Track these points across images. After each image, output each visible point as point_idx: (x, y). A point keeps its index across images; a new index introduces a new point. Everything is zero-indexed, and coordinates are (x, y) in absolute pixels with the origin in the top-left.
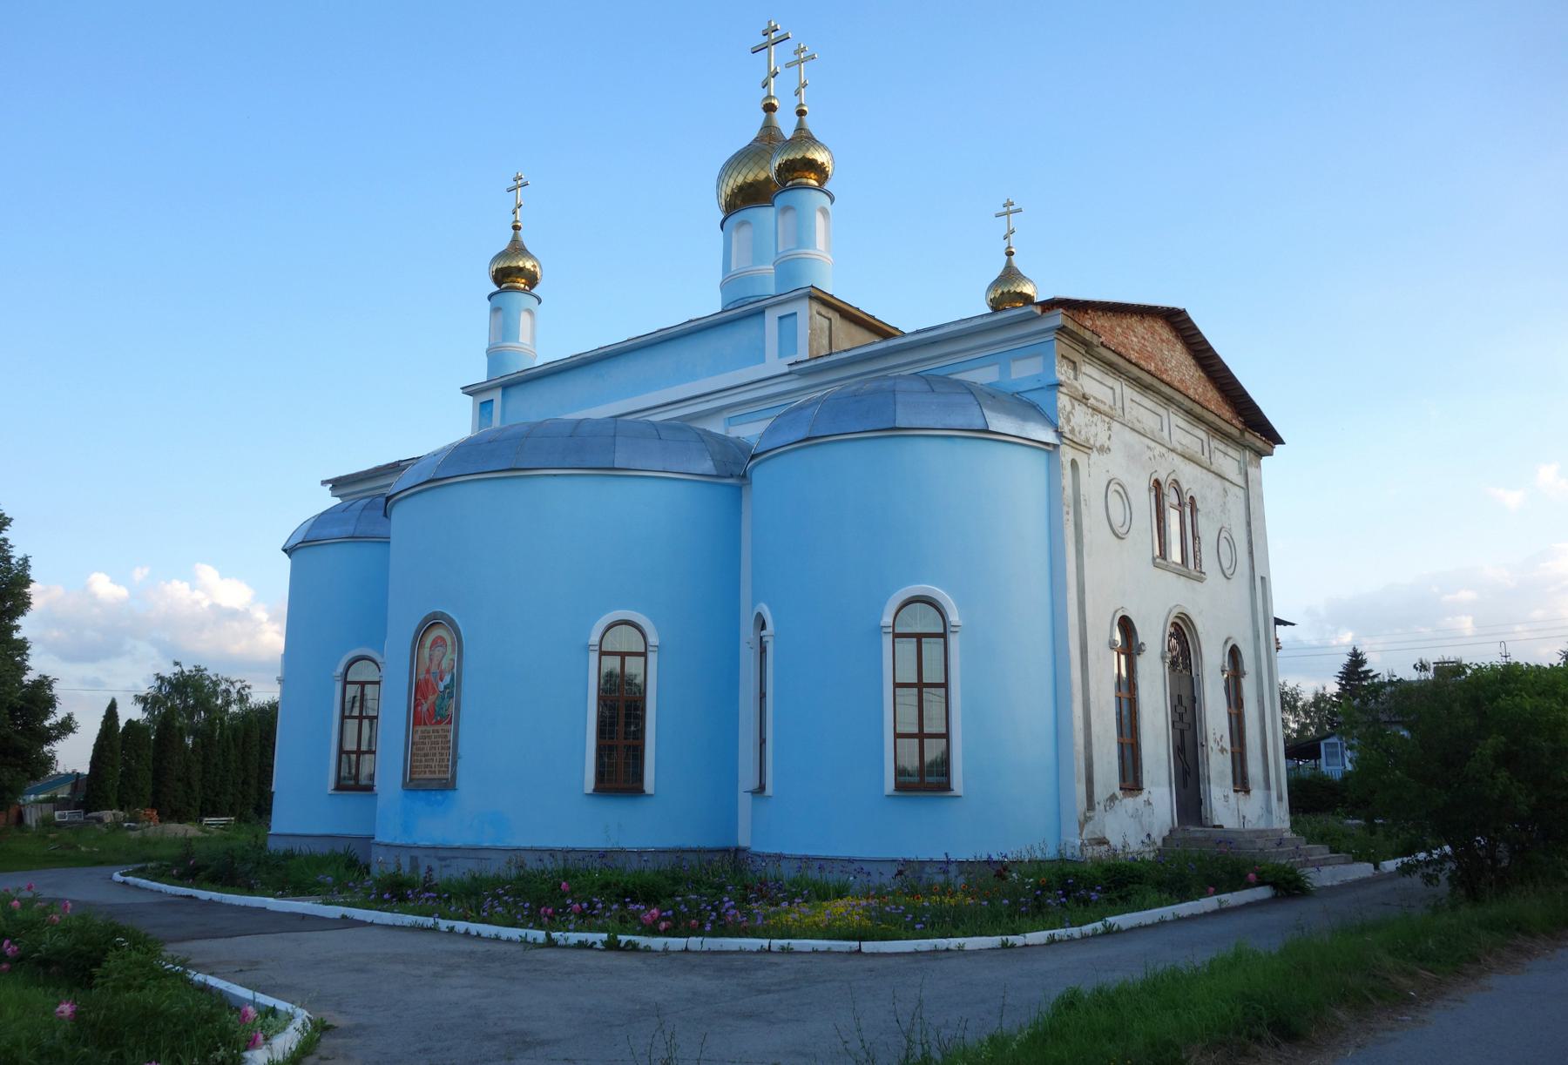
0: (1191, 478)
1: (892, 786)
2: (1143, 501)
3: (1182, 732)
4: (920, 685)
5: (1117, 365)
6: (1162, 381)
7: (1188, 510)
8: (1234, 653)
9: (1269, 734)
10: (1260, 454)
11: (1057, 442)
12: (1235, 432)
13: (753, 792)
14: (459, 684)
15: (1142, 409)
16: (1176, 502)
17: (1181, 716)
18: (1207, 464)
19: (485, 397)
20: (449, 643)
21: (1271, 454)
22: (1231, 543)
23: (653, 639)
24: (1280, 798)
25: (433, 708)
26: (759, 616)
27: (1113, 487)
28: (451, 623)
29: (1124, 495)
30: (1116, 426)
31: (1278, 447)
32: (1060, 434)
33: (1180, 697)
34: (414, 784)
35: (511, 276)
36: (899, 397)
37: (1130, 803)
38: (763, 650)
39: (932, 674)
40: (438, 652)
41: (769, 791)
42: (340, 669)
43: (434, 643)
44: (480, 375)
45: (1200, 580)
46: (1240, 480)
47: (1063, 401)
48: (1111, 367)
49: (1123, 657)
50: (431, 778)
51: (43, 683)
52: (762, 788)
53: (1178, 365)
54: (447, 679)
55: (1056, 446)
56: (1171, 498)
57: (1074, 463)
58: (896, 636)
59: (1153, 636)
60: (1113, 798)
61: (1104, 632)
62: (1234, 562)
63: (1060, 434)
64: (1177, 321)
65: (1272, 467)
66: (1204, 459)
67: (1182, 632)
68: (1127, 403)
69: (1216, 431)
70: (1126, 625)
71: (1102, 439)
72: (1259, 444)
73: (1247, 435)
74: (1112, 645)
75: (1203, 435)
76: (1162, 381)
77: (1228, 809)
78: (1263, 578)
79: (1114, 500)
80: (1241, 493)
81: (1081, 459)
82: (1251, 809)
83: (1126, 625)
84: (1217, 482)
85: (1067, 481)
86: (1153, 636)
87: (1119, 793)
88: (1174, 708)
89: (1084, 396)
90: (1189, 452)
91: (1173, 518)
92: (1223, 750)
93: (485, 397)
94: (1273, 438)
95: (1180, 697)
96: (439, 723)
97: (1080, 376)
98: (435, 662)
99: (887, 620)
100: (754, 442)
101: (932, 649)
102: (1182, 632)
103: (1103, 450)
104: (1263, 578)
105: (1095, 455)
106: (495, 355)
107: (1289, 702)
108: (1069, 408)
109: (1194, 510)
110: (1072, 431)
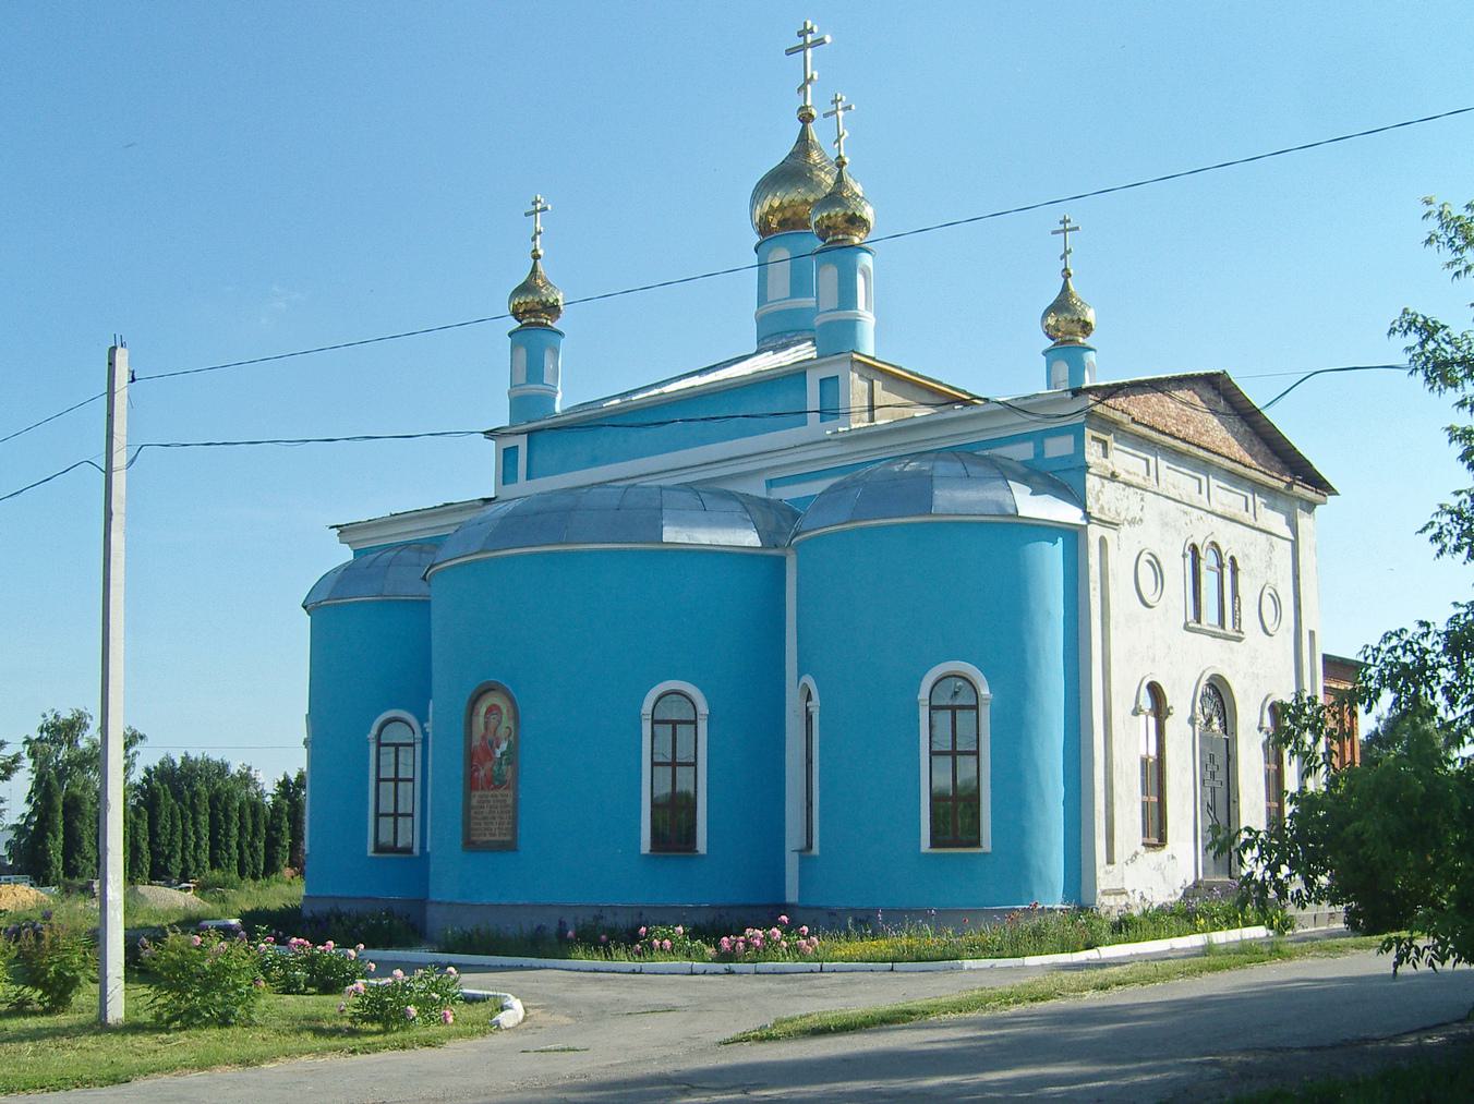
0: (1233, 540)
1: (649, 848)
2: (1177, 571)
3: (1213, 790)
4: (954, 753)
5: (1143, 441)
7: (1227, 572)
10: (1310, 506)
11: (1084, 523)
12: (1282, 485)
13: (800, 851)
16: (1214, 564)
18: (1251, 521)
19: (509, 442)
20: (505, 711)
23: (703, 708)
27: (1145, 557)
28: (506, 693)
29: (1156, 564)
32: (1087, 516)
33: (1212, 758)
35: (534, 314)
36: (935, 482)
37: (1154, 857)
40: (493, 720)
42: (374, 732)
43: (489, 711)
44: (502, 419)
45: (1239, 640)
46: (1287, 532)
47: (1092, 482)
51: (186, 759)
53: (1217, 433)
54: (504, 746)
56: (1208, 559)
59: (1181, 701)
63: (1087, 516)
64: (1218, 389)
66: (1248, 518)
69: (1257, 487)
70: (1155, 690)
71: (1135, 512)
72: (1310, 495)
76: (1199, 446)
81: (1109, 534)
84: (1264, 535)
86: (1181, 701)
88: (1204, 765)
90: (1229, 512)
91: (1209, 581)
93: (509, 442)
96: (496, 788)
98: (491, 729)
102: (1218, 694)
104: (1312, 634)
105: (1125, 529)
106: (519, 404)
108: (1098, 487)
109: (1235, 571)
110: (1102, 509)
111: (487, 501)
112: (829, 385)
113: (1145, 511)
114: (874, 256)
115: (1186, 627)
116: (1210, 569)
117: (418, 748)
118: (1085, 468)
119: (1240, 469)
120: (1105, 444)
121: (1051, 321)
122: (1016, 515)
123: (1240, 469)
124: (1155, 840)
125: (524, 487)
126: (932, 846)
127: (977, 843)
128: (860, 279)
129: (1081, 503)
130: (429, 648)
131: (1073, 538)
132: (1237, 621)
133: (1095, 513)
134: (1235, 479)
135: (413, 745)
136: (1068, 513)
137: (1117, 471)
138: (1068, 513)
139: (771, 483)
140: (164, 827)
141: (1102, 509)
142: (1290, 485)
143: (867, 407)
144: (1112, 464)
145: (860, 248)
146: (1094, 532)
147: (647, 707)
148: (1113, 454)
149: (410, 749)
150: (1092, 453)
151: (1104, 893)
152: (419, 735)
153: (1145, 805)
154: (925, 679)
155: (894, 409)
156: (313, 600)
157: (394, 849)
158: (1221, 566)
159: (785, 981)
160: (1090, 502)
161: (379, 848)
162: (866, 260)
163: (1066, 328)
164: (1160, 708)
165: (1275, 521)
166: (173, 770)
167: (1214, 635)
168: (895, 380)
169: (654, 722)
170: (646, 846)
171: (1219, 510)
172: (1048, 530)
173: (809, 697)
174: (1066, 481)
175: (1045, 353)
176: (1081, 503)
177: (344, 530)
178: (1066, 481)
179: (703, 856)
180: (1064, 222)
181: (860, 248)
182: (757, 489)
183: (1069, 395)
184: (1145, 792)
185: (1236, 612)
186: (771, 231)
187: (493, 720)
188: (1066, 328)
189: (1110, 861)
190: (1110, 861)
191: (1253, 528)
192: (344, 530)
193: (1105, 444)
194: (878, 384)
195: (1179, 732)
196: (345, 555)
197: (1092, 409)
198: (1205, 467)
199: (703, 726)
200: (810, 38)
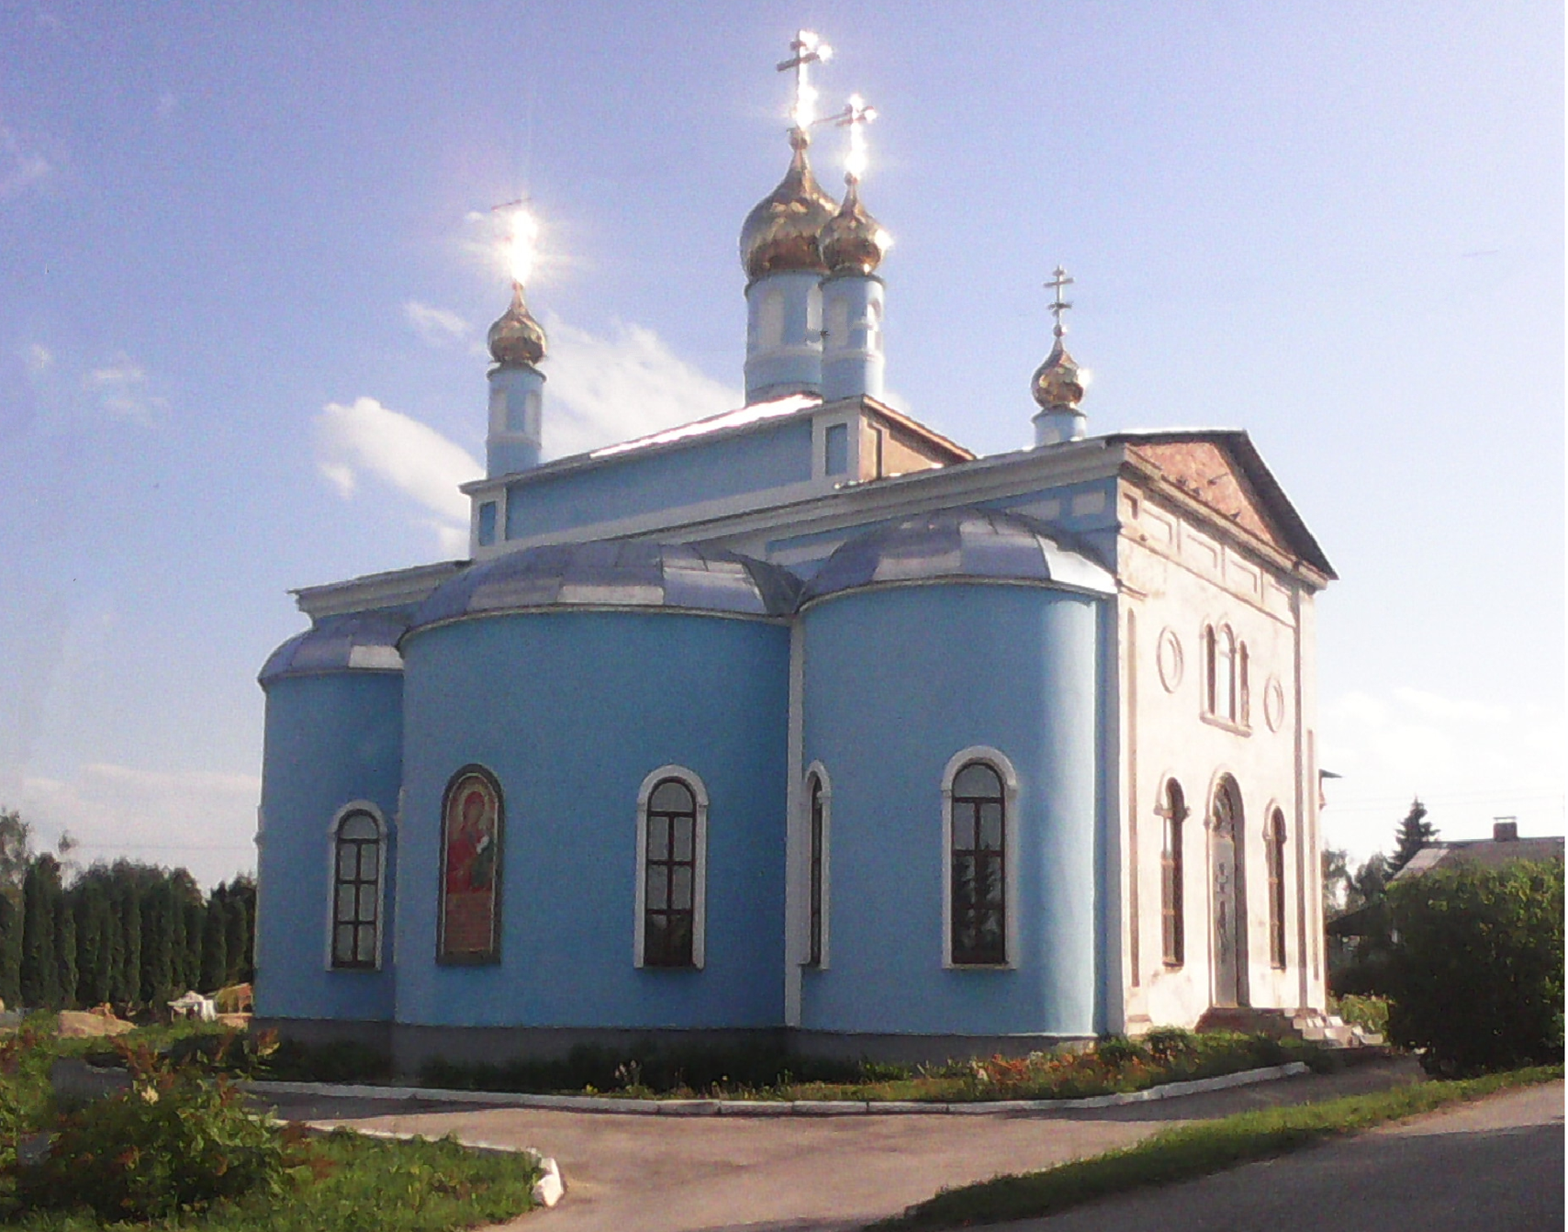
3: (1222, 904)
6: (1218, 512)
8: (1278, 818)
9: (1314, 902)
10: (1312, 589)
11: (1114, 590)
12: (1288, 565)
14: (501, 850)
15: (1198, 547)
17: (1222, 888)
21: (1323, 588)
22: (1280, 695)
23: (702, 799)
24: (1316, 976)
25: (470, 873)
26: (814, 774)
27: (1168, 635)
30: (1171, 566)
31: (1331, 583)
32: (1119, 583)
34: (447, 959)
38: (817, 813)
39: (348, 892)
41: (824, 966)
42: (335, 826)
43: (469, 800)
45: (1246, 735)
47: (1123, 544)
48: (1167, 503)
49: (1168, 823)
50: (469, 948)
52: (816, 959)
53: (1233, 496)
54: (485, 840)
55: (1114, 598)
56: (1223, 645)
57: (1131, 615)
58: (956, 800)
60: (1156, 975)
61: (1151, 795)
62: (1281, 713)
63: (1119, 583)
64: (1235, 448)
65: (1320, 606)
66: (1256, 598)
67: (1229, 793)
68: (1184, 538)
69: (1267, 565)
70: (1174, 790)
72: (1313, 576)
73: (1302, 570)
74: (1158, 810)
75: (1257, 570)
76: (1218, 512)
77: (1271, 989)
78: (1310, 733)
79: (1167, 652)
80: (1290, 632)
81: (1136, 605)
82: (1287, 987)
83: (1174, 790)
84: (1270, 620)
85: (1123, 634)
86: (1199, 802)
87: (1162, 968)
89: (1143, 538)
91: (1222, 665)
92: (1261, 924)
94: (1326, 570)
95: (1222, 867)
96: (476, 890)
97: (1141, 515)
99: (947, 784)
100: (806, 576)
101: (989, 812)
102: (1229, 793)
103: (1158, 594)
104: (1310, 733)
105: (1149, 600)
107: (1332, 866)
109: (1245, 657)
111: (460, 564)
112: (837, 432)
113: (1170, 580)
114: (884, 287)
115: (1203, 719)
116: (1222, 653)
117: (383, 846)
118: (1117, 527)
119: (1254, 542)
120: (1134, 503)
121: (1042, 383)
122: (1048, 579)
123: (1254, 542)
124: (1172, 959)
125: (503, 548)
126: (955, 960)
127: (1002, 959)
128: (870, 310)
129: (1111, 567)
130: (828, 441)
131: (1106, 606)
132: (1246, 714)
133: (1125, 582)
134: (1248, 552)
135: (376, 842)
136: (1095, 578)
137: (1147, 535)
138: (1095, 578)
139: (772, 547)
140: (92, 940)
141: (1130, 579)
142: (1296, 565)
143: (879, 458)
144: (1143, 522)
145: (871, 277)
146: (1125, 603)
147: (643, 796)
148: (1142, 516)
149: (373, 847)
150: (1123, 511)
151: (1131, 1020)
152: (383, 829)
153: (1165, 918)
154: (948, 767)
155: (903, 462)
156: (266, 675)
157: (355, 963)
158: (1233, 651)
159: (843, 1127)
160: (1120, 568)
161: (337, 962)
162: (876, 291)
163: (1057, 392)
164: (1177, 812)
165: (1278, 599)
166: (108, 878)
167: (1226, 728)
168: (900, 431)
169: (651, 814)
170: (639, 962)
171: (1233, 589)
172: (1084, 595)
173: (817, 786)
174: (1096, 543)
175: (1036, 419)
176: (1111, 567)
177: (306, 598)
178: (1096, 543)
179: (700, 971)
180: (1059, 273)
181: (871, 277)
182: (758, 553)
183: (1103, 444)
184: (1165, 904)
185: (1246, 703)
186: (762, 269)
187: (473, 812)
188: (1057, 392)
189: (1136, 983)
190: (1136, 983)
191: (1260, 610)
192: (306, 598)
193: (1134, 503)
194: (886, 432)
195: (1196, 832)
196: (305, 623)
197: (1121, 461)
198: (1222, 536)
199: (701, 820)
200: (803, 53)
